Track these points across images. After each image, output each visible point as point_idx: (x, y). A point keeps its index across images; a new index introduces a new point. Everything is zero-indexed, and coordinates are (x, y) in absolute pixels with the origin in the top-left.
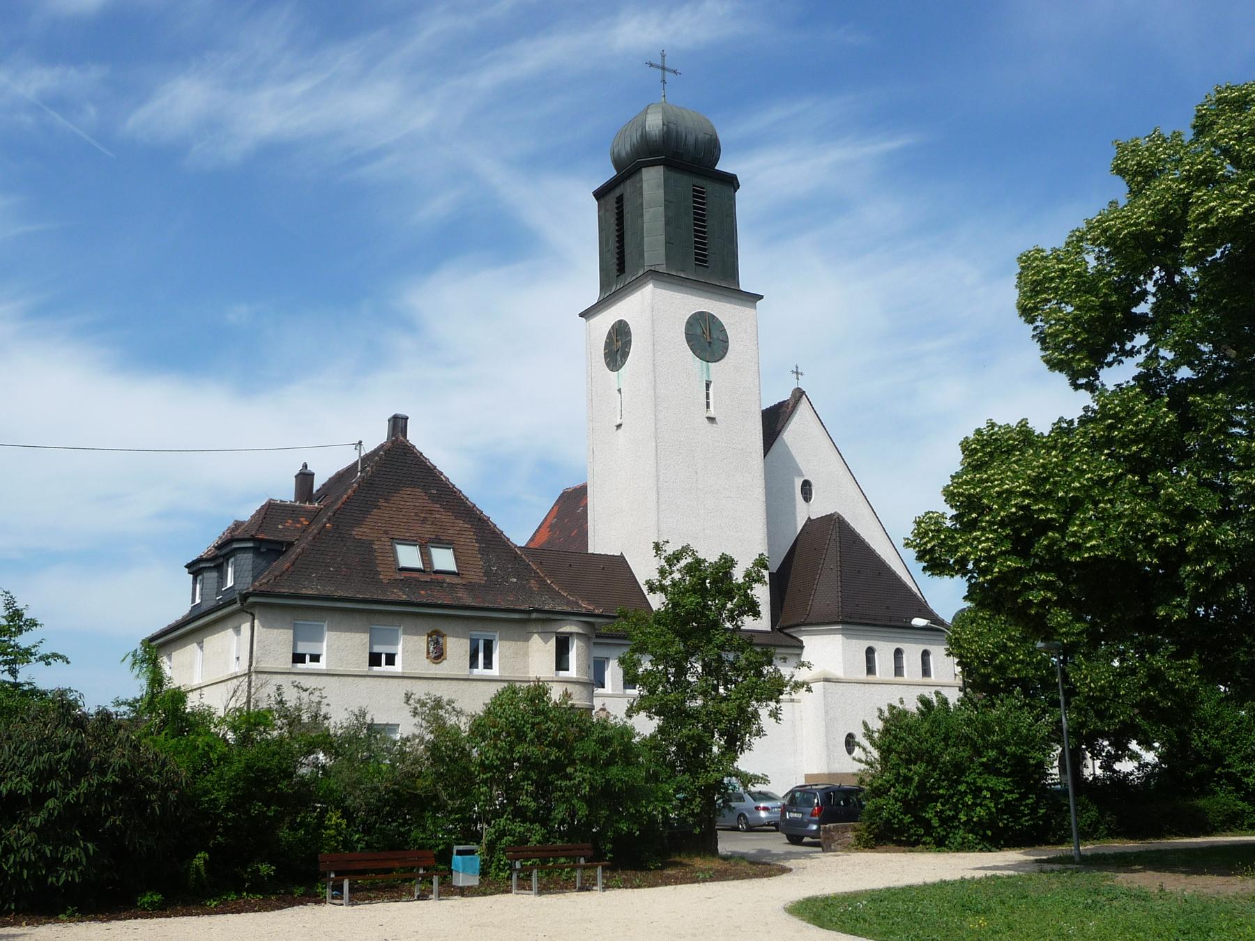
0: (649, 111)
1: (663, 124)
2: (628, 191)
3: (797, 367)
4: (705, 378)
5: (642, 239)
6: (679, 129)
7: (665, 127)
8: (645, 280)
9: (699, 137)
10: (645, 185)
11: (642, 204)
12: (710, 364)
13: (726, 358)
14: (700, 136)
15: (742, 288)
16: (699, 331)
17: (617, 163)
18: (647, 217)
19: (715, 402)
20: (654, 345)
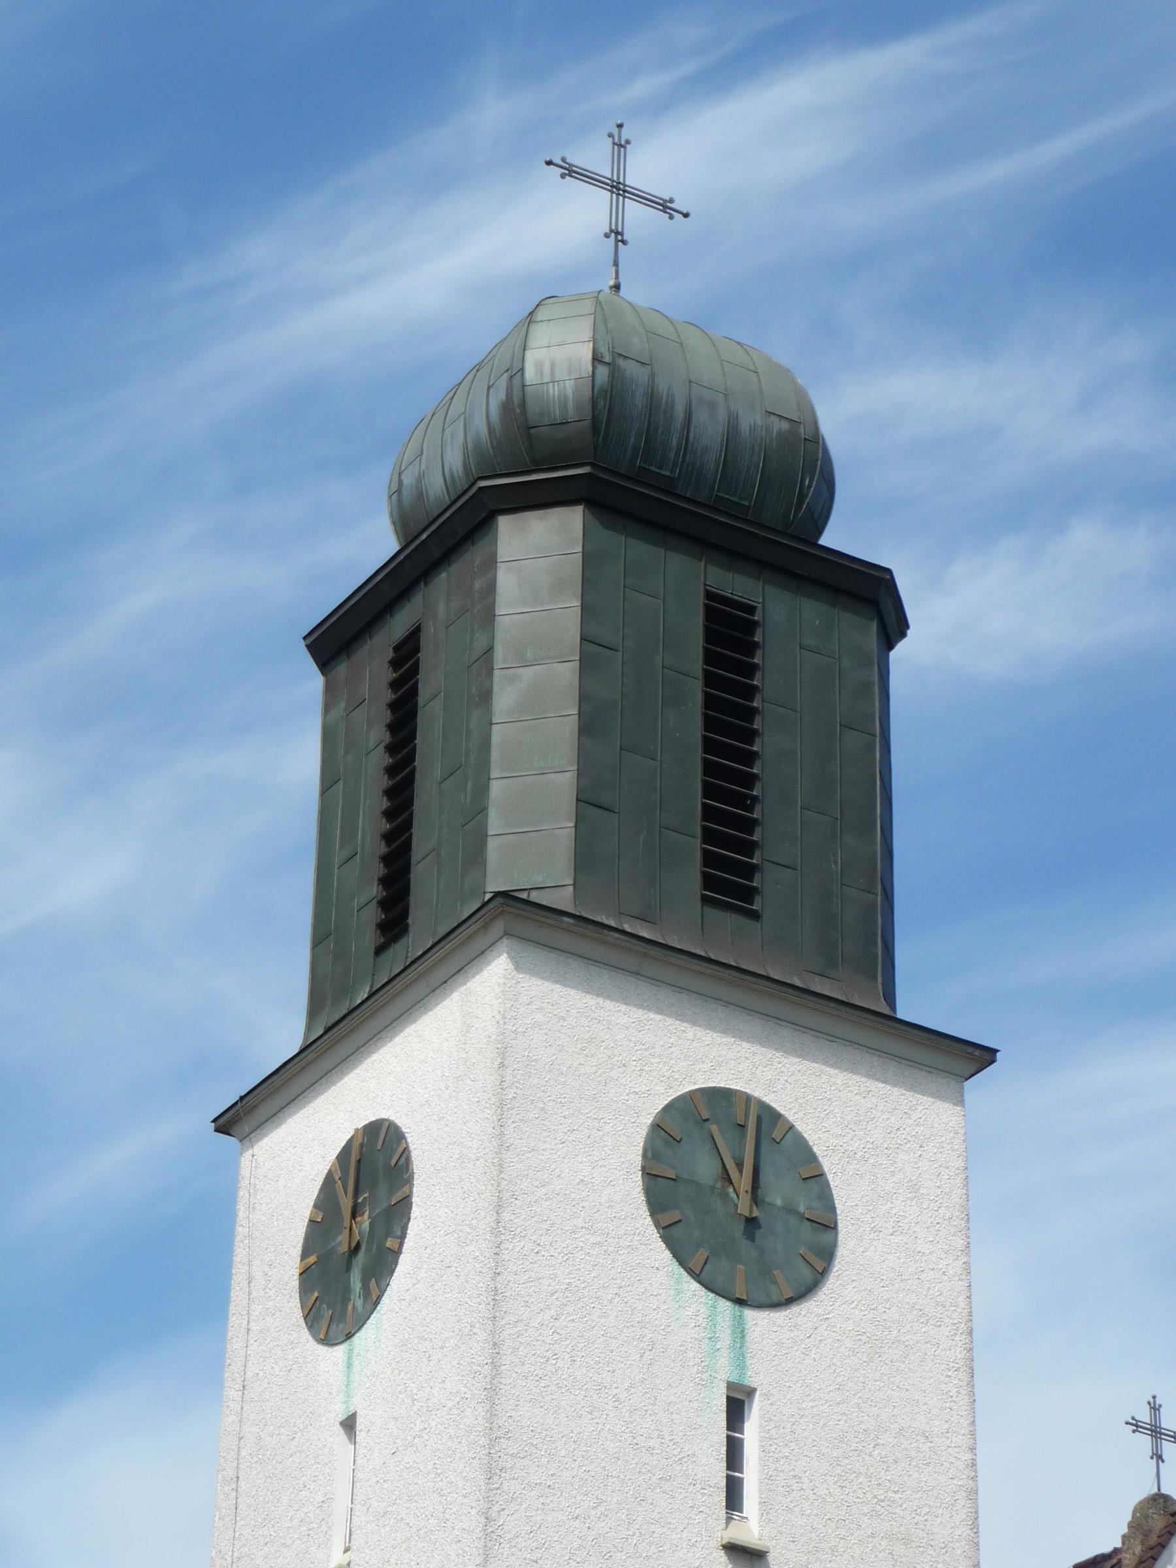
0: (539, 316)
1: (596, 359)
2: (442, 607)
3: (1155, 1408)
4: (724, 1372)
5: (482, 790)
6: (662, 385)
7: (603, 372)
8: (480, 942)
9: (746, 423)
10: (505, 580)
11: (490, 650)
12: (749, 1314)
13: (832, 1283)
14: (750, 420)
15: (901, 1014)
16: (705, 1169)
17: (404, 523)
18: (504, 699)
19: (767, 1480)
20: (499, 1208)
